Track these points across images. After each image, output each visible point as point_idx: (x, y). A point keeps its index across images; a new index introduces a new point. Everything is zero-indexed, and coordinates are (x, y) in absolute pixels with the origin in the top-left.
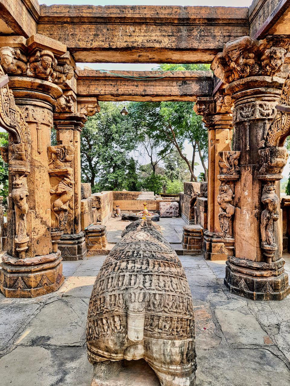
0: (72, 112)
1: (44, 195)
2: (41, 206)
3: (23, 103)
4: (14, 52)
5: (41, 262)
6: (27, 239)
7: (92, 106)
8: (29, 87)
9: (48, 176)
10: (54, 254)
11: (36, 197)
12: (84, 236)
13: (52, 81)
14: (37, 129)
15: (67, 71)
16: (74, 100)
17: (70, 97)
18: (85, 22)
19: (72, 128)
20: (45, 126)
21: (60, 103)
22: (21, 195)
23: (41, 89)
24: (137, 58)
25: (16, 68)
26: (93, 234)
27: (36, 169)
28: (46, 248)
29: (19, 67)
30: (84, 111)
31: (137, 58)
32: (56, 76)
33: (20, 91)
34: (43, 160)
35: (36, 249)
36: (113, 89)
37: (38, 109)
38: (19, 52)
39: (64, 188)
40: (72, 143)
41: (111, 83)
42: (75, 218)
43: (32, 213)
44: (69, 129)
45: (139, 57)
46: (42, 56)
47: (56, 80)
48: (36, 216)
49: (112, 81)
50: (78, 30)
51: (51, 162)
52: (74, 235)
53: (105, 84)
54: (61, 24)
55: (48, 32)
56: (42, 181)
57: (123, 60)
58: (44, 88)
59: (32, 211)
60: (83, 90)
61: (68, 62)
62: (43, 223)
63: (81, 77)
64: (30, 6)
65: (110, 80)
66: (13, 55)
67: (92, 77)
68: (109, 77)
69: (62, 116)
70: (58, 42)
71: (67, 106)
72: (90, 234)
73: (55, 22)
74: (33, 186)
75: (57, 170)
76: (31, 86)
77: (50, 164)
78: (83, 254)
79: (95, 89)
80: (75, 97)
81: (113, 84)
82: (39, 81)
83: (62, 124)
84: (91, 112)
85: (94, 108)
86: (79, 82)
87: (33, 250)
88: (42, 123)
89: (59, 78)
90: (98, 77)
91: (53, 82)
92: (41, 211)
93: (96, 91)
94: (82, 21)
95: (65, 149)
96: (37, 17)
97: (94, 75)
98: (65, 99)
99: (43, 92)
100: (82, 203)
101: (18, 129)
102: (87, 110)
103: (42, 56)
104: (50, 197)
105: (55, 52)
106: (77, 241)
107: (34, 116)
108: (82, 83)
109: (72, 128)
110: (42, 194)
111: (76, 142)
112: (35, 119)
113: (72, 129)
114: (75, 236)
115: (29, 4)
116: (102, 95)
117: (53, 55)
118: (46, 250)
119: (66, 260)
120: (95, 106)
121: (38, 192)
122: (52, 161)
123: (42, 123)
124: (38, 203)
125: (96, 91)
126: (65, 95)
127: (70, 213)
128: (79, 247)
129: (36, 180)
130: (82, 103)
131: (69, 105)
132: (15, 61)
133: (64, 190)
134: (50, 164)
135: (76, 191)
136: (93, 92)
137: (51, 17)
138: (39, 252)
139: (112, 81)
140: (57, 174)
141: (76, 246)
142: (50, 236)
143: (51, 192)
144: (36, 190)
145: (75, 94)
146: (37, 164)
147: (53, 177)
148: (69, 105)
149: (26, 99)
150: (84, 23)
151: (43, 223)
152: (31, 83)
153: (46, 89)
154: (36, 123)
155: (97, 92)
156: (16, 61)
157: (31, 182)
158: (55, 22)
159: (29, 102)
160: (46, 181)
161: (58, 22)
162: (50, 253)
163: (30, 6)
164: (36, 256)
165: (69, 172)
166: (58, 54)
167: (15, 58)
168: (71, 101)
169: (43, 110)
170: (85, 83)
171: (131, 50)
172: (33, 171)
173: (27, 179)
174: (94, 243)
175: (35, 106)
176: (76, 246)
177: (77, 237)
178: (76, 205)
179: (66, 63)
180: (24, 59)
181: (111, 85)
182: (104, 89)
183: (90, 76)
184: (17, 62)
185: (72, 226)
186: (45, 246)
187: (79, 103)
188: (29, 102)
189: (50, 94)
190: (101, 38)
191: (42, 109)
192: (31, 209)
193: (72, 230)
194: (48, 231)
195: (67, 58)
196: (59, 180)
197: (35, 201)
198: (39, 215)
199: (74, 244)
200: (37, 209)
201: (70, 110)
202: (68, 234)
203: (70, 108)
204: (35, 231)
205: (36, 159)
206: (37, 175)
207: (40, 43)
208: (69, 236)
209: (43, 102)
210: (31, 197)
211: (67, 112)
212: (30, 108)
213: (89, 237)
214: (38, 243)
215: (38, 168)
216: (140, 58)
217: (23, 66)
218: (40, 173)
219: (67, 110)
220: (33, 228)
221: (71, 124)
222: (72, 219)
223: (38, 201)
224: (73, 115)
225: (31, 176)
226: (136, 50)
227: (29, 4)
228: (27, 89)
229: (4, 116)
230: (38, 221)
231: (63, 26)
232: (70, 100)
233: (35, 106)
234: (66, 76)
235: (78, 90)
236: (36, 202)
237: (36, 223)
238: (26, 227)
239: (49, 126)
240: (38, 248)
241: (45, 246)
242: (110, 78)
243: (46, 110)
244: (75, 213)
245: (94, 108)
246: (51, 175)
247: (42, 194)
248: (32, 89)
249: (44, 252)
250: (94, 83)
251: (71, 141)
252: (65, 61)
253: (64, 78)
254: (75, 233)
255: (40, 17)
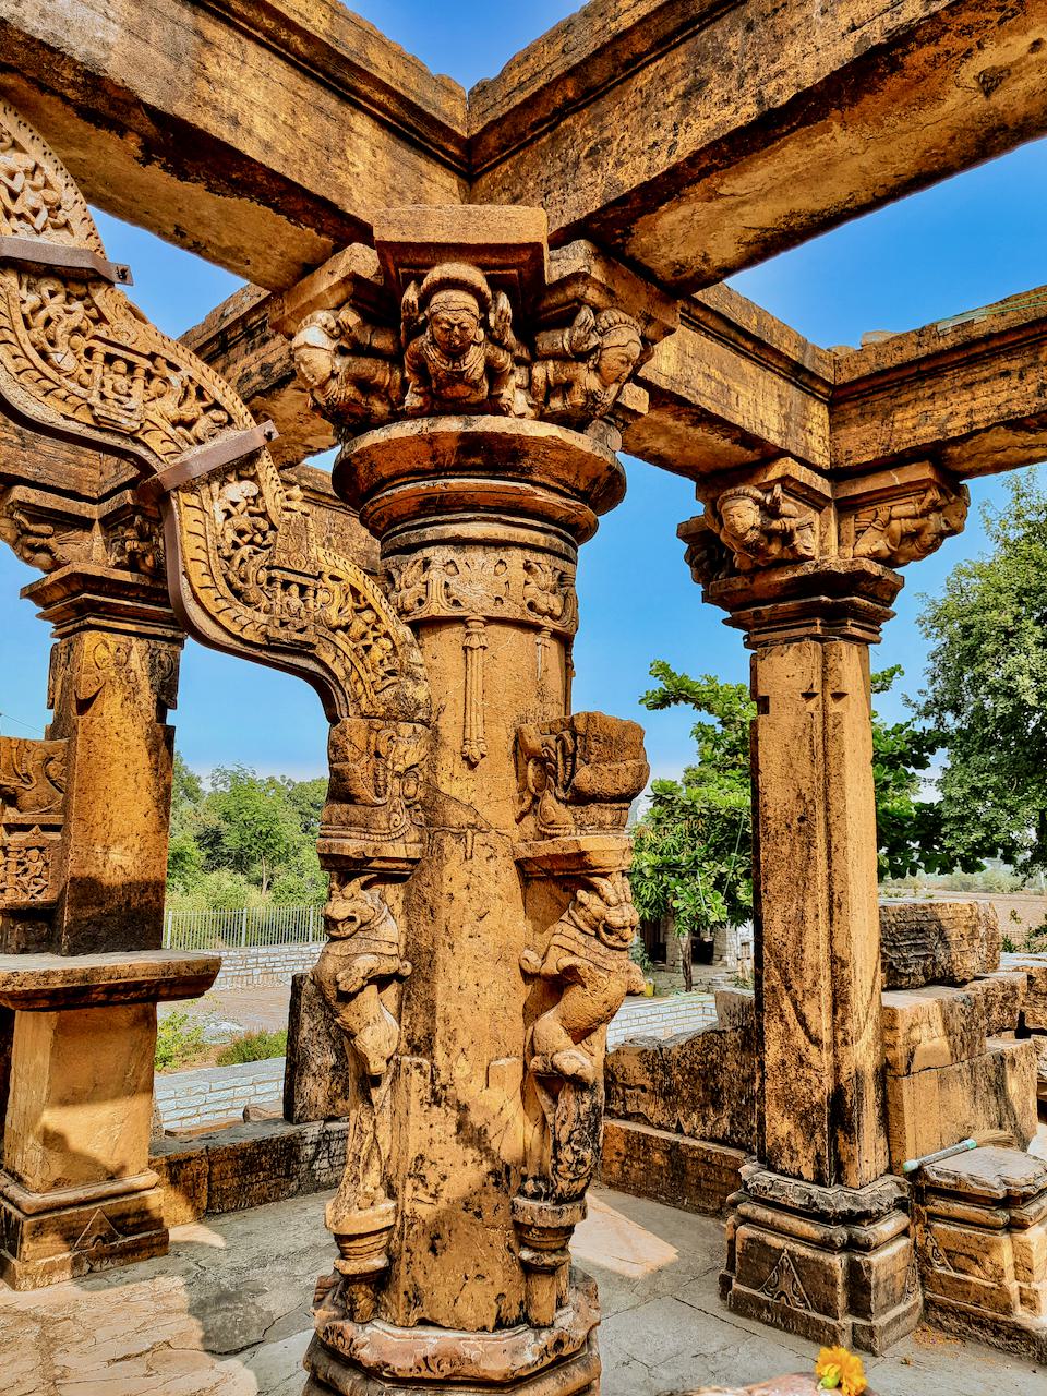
0: (806, 558)
1: (484, 982)
2: (463, 1039)
3: (414, 540)
4: (332, 324)
5: (426, 1374)
6: (380, 1213)
7: (910, 509)
8: (427, 464)
9: (510, 879)
10: (530, 1335)
11: (440, 987)
12: (901, 1205)
13: (532, 412)
14: (465, 648)
15: (594, 341)
16: (814, 500)
17: (778, 489)
18: (642, 55)
19: (812, 630)
20: (513, 633)
21: (732, 526)
22: (340, 977)
23: (478, 461)
24: (979, 103)
25: (350, 391)
26: (959, 1209)
27: (449, 843)
28: (474, 1288)
29: (363, 385)
30: (874, 542)
31: (979, 103)
32: (547, 382)
33: (393, 491)
34: (487, 795)
35: (421, 1283)
36: (1016, 394)
37: (477, 556)
38: (350, 317)
39: (572, 945)
40: (812, 703)
41: (1005, 366)
42: (838, 1095)
43: (416, 1073)
44: (799, 639)
45: (987, 93)
46: (425, 300)
47: (556, 404)
48: (434, 1094)
49: (1007, 353)
50: (613, 118)
51: (524, 807)
52: (832, 1192)
53: (969, 379)
54: (550, 129)
55: (505, 197)
56: (476, 905)
57: (907, 167)
58: (490, 451)
59: (417, 1060)
60: (863, 440)
61: (592, 295)
62: (472, 1136)
63: (845, 386)
64: (392, 106)
65: (994, 354)
66: (334, 338)
67: (899, 368)
68: (989, 337)
69: (762, 582)
70: (513, 208)
71: (770, 535)
72: (940, 1206)
73: (523, 135)
74: (430, 929)
75: (546, 848)
76: (433, 458)
77: (523, 814)
78: (880, 1321)
79: (916, 422)
80: (821, 485)
81: (1016, 365)
82: (452, 425)
83: (771, 623)
84: (912, 536)
85: (925, 514)
86: (842, 413)
87: (404, 1283)
88: (490, 621)
89: (564, 388)
90: (928, 358)
91: (542, 417)
92: (462, 1069)
93: (921, 432)
94: (626, 56)
95: (574, 735)
96: (452, 149)
97: (911, 353)
98: (757, 501)
99: (492, 470)
100: (888, 1020)
101: (327, 658)
102: (890, 535)
103: (425, 300)
104: (525, 991)
105: (486, 259)
106: (840, 1234)
107: (452, 590)
108: (854, 412)
109: (812, 630)
110: (470, 976)
111: (838, 696)
112: (456, 603)
113: (815, 638)
114: (833, 1198)
115: (380, 97)
116: (955, 441)
117: (477, 278)
118: (479, 1302)
119: (789, 1331)
120: (925, 505)
121: (453, 964)
122: (528, 799)
123: (490, 621)
124: (446, 1021)
125: (921, 432)
126: (758, 487)
127: (810, 1066)
128: (854, 1270)
129: (443, 901)
130: (863, 506)
131: (776, 525)
132: (341, 363)
133: (568, 961)
134: (523, 814)
135: (839, 944)
136: (906, 437)
137: (505, 117)
138: (438, 1306)
139: (1010, 351)
140: (547, 866)
141: (838, 1262)
142: (502, 1218)
143: (527, 967)
144: (442, 954)
145: (817, 469)
146: (457, 816)
147: (537, 886)
148: (776, 525)
149: (422, 521)
150: (634, 65)
151: (472, 1136)
152: (425, 446)
153: (502, 455)
154: (462, 621)
155: (927, 433)
156: (348, 359)
157: (420, 908)
158: (523, 135)
159: (431, 533)
160: (496, 906)
161: (535, 126)
162: (500, 1324)
163: (392, 106)
164: (423, 1322)
165: (595, 860)
166: (515, 273)
167: (341, 351)
168: (787, 506)
169: (502, 555)
170: (868, 407)
171: (896, 67)
172: (434, 851)
173: (408, 892)
174: (961, 1261)
175: (460, 543)
176: (838, 1262)
177: (844, 1207)
178: (843, 1021)
179: (580, 302)
180: (382, 342)
181: (1006, 374)
182: (963, 409)
183: (889, 364)
184: (349, 366)
185: (818, 1136)
186: (471, 1273)
187: (846, 508)
188: (431, 533)
189: (537, 478)
190: (716, 90)
191: (495, 555)
192: (416, 1049)
193: (818, 1159)
194: (491, 1189)
195: (576, 277)
196: (559, 903)
197: (434, 1007)
198: (451, 1090)
199: (826, 1245)
200: (439, 1052)
201: (793, 549)
202: (800, 1177)
203: (786, 537)
204: (422, 1178)
205: (455, 793)
206: (454, 872)
207: (404, 239)
208: (803, 1194)
209: (499, 521)
210: (420, 988)
211: (780, 564)
212: (439, 555)
213: (933, 1216)
214: (433, 1249)
215: (460, 836)
216: (999, 99)
217: (383, 375)
218: (468, 865)
219: (775, 549)
220: (412, 1155)
221: (807, 613)
222: (817, 1097)
223: (451, 1008)
224: (808, 568)
225: (425, 879)
226: (930, 51)
227: (380, 97)
228: (423, 474)
229: (222, 604)
230: (444, 1122)
231: (558, 135)
232: (776, 501)
233: (460, 543)
234: (597, 369)
235: (834, 449)
236: (439, 1014)
237: (430, 1131)
238: (385, 1150)
239: (537, 629)
240: (437, 1278)
241: (471, 1273)
242: (997, 343)
243: (516, 557)
244: (837, 1068)
245: (925, 514)
246: (526, 870)
247: (470, 976)
248: (439, 471)
249: (466, 1311)
250: (911, 396)
251: (808, 696)
252: (570, 293)
253: (592, 382)
254: (840, 1181)
255: (470, 145)
